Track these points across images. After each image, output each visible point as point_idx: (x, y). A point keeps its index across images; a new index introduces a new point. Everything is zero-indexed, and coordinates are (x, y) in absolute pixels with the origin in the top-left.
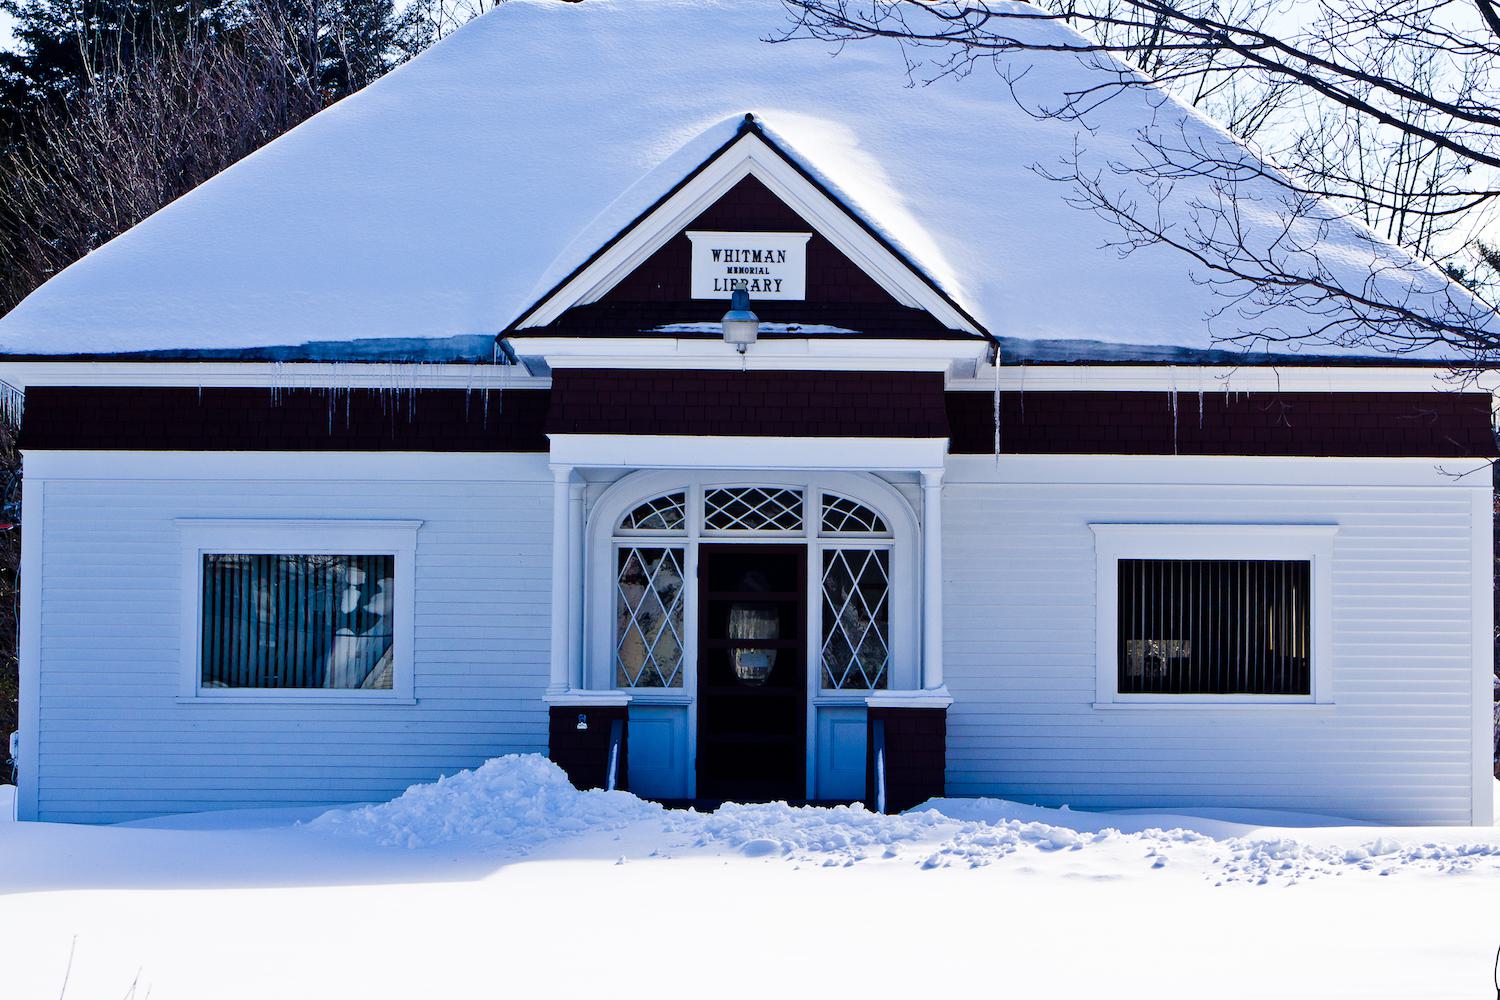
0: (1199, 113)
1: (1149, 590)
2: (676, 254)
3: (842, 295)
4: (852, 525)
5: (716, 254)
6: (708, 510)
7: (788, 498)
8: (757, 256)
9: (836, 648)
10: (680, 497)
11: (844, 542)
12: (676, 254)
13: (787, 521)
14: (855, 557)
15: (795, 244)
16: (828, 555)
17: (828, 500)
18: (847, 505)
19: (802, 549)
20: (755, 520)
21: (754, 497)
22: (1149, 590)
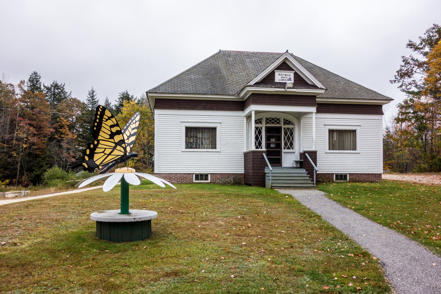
0: (66, 130)
1: (191, 132)
2: (271, 75)
3: (299, 81)
4: (288, 124)
5: (279, 75)
6: (266, 121)
7: (278, 119)
8: (286, 75)
9: (286, 144)
10: (261, 119)
11: (287, 126)
12: (271, 75)
13: (278, 123)
14: (288, 129)
15: (291, 75)
16: (284, 128)
17: (284, 120)
18: (287, 121)
19: (281, 127)
20: (273, 123)
21: (273, 119)
22: (191, 132)
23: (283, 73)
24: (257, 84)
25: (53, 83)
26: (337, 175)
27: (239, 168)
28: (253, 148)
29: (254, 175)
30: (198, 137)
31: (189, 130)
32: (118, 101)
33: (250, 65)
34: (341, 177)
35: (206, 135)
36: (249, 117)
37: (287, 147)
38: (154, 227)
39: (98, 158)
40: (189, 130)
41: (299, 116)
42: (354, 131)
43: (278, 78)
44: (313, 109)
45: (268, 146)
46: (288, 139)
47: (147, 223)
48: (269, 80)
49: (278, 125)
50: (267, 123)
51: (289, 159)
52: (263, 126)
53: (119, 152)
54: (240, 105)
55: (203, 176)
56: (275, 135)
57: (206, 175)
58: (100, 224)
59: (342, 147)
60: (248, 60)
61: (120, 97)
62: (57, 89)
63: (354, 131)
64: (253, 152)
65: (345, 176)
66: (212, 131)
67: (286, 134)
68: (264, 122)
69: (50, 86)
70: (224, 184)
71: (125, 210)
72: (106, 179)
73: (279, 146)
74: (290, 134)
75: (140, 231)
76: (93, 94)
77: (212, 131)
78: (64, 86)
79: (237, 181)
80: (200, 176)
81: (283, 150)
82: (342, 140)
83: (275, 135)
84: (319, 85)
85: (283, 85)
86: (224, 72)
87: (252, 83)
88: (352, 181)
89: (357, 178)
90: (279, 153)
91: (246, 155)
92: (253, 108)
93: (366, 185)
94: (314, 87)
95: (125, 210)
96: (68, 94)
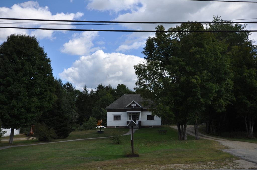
2: (131, 105)
9: (137, 119)
12: (131, 105)
24: (127, 107)
25: (67, 83)
28: (128, 121)
30: (117, 118)
32: (97, 88)
37: (137, 119)
39: (98, 125)
43: (132, 105)
44: (140, 112)
47: (103, 132)
49: (135, 115)
50: (132, 114)
53: (100, 124)
54: (125, 110)
58: (98, 132)
61: (97, 87)
62: (68, 86)
66: (120, 116)
68: (132, 114)
69: (65, 84)
71: (101, 130)
76: (85, 88)
77: (120, 116)
78: (72, 84)
81: (136, 120)
84: (141, 107)
87: (126, 107)
92: (127, 112)
94: (140, 107)
95: (101, 130)
96: (74, 88)
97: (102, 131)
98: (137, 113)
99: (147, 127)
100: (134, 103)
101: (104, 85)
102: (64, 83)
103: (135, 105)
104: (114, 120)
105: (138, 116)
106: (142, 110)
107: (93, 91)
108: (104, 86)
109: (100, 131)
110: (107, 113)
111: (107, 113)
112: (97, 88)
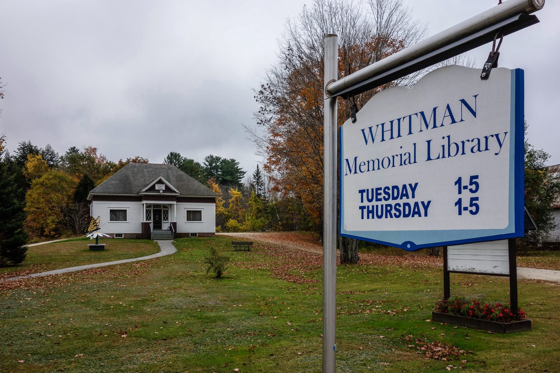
2: (154, 186)
9: (164, 218)
12: (154, 186)
15: (164, 186)
23: (160, 185)
24: (146, 191)
26: (191, 234)
27: (139, 231)
28: (145, 221)
29: (145, 235)
30: (118, 215)
31: (112, 211)
33: (146, 174)
34: (194, 234)
35: (121, 213)
36: (143, 205)
38: (105, 248)
39: (89, 230)
40: (112, 211)
41: (171, 205)
42: (200, 212)
43: (157, 187)
44: (175, 203)
45: (154, 219)
46: (166, 215)
47: (103, 246)
48: (153, 188)
51: (165, 226)
52: (152, 209)
54: (138, 199)
55: (120, 235)
56: (158, 215)
57: (121, 235)
58: (90, 246)
59: (194, 219)
60: (145, 170)
63: (200, 212)
64: (145, 223)
65: (196, 234)
67: (164, 212)
68: (152, 207)
70: (131, 239)
71: (97, 243)
72: (180, 237)
73: (160, 219)
74: (166, 213)
75: (102, 248)
79: (137, 237)
80: (118, 235)
82: (194, 216)
83: (158, 215)
84: (177, 191)
85: (158, 191)
86: (131, 178)
87: (144, 190)
88: (199, 236)
89: (202, 235)
90: (161, 223)
91: (142, 223)
92: (144, 202)
93: (206, 238)
94: (175, 192)
95: (97, 243)
97: (99, 244)
98: (165, 206)
99: (186, 235)
100: (160, 182)
101: (34, 146)
102: (61, 151)
103: (163, 187)
104: (111, 220)
105: (167, 213)
106: (180, 199)
107: (10, 155)
108: (35, 147)
109: (94, 244)
110: (514, 232)
111: (514, 232)
112: (19, 149)
